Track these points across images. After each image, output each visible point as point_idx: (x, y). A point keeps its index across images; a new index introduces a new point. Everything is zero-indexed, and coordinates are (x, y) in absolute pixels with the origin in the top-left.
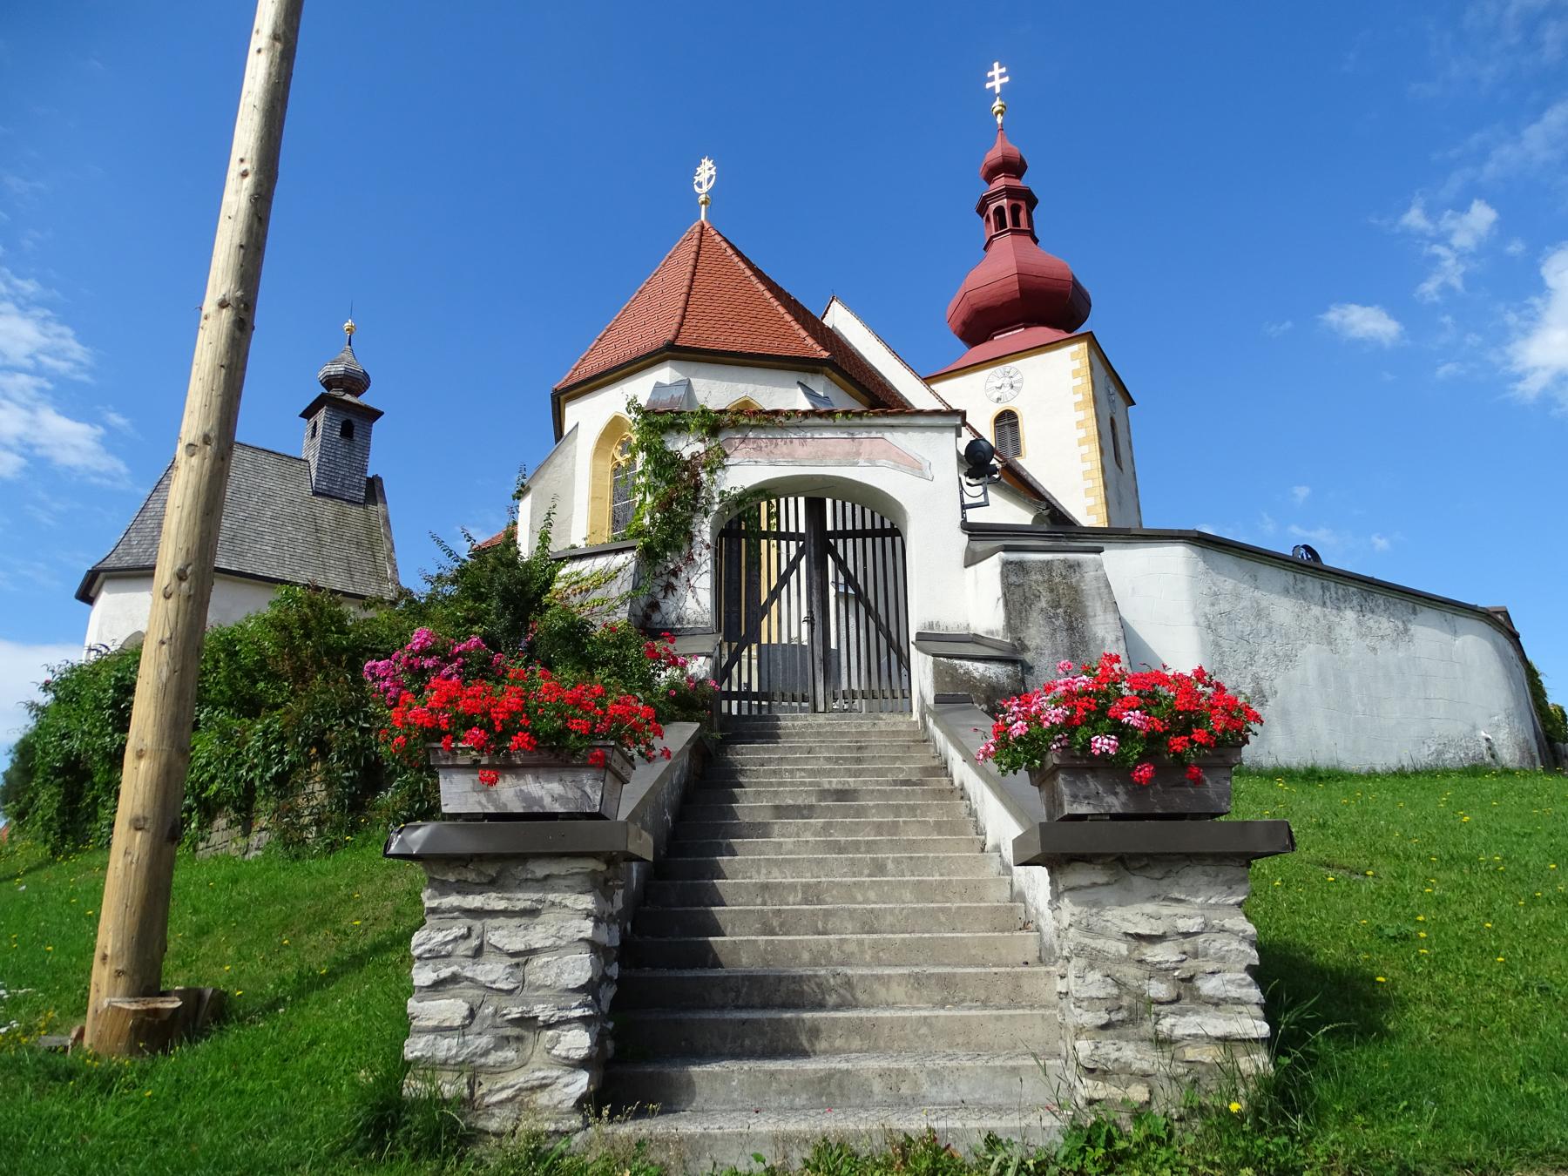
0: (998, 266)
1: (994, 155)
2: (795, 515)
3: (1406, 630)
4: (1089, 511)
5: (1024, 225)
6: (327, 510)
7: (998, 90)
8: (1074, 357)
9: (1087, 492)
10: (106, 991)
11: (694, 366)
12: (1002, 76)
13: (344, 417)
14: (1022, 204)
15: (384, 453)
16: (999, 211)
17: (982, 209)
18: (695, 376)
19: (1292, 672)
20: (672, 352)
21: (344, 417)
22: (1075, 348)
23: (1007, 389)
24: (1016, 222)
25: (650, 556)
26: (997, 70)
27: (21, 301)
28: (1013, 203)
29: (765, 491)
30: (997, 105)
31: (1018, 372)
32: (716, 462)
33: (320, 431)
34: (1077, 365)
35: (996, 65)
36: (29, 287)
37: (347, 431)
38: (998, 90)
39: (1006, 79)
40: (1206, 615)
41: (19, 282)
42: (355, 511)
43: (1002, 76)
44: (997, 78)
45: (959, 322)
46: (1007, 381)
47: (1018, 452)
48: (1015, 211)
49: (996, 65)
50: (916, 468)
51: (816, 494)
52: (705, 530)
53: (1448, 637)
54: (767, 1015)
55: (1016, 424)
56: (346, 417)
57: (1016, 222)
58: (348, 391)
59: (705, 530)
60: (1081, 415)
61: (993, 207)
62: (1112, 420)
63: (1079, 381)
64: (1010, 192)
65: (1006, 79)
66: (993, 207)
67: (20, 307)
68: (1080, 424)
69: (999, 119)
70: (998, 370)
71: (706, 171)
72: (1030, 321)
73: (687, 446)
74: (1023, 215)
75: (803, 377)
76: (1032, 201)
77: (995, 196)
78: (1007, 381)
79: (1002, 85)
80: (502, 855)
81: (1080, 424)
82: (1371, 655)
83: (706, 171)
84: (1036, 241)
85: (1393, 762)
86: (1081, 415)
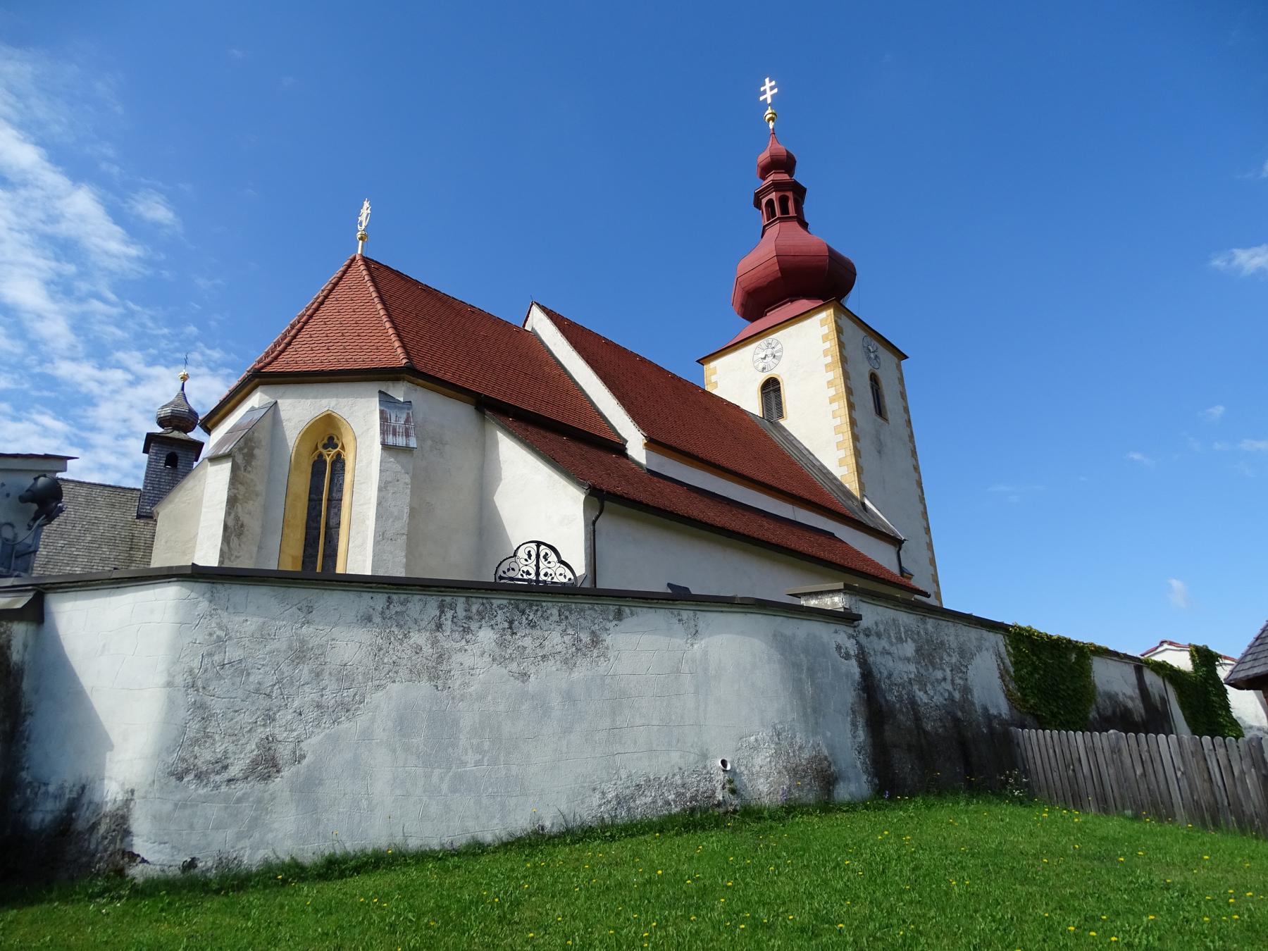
0: (761, 250)
1: (764, 157)
3: (596, 640)
4: (841, 462)
5: (792, 212)
7: (769, 101)
8: (823, 323)
9: (839, 446)
11: (281, 389)
12: (772, 88)
14: (790, 194)
16: (770, 202)
17: (758, 204)
18: (281, 397)
19: (346, 725)
22: (823, 315)
23: (769, 359)
24: (785, 210)
26: (768, 84)
27: (212, 365)
28: (784, 193)
30: (768, 113)
31: (778, 342)
34: (825, 330)
35: (767, 80)
36: (216, 354)
38: (769, 101)
39: (776, 91)
40: (191, 671)
41: (208, 352)
43: (772, 88)
44: (769, 90)
45: (738, 305)
46: (769, 352)
47: (781, 415)
48: (783, 201)
49: (767, 80)
53: (678, 641)
55: (779, 390)
56: (171, 451)
57: (785, 210)
58: (176, 428)
60: (831, 376)
61: (764, 201)
62: (874, 379)
63: (827, 345)
64: (776, 186)
65: (776, 91)
66: (764, 201)
67: (211, 369)
68: (830, 384)
69: (771, 125)
70: (762, 343)
72: (794, 296)
74: (791, 205)
75: (383, 386)
76: (800, 192)
77: (765, 191)
78: (769, 352)
79: (772, 96)
81: (830, 384)
82: (518, 684)
84: (804, 225)
85: (520, 823)
86: (831, 376)
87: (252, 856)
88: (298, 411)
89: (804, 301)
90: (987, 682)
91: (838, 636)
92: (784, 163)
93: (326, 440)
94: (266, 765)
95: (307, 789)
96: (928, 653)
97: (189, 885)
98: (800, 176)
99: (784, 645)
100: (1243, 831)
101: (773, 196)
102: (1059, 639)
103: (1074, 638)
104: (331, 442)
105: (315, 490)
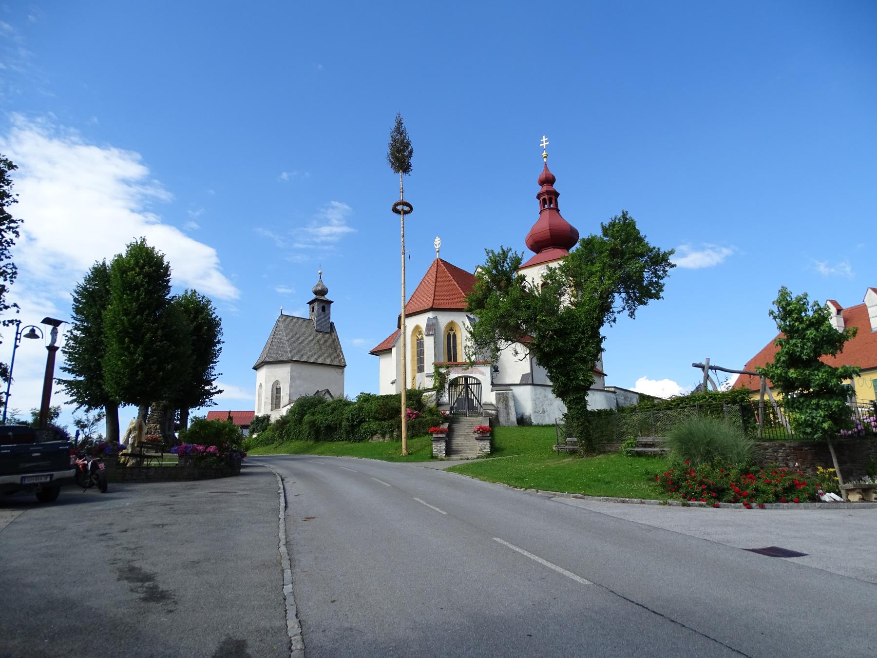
2: (462, 381)
6: (320, 336)
10: (404, 451)
13: (322, 305)
14: (553, 197)
15: (335, 315)
17: (538, 197)
20: (432, 309)
21: (322, 305)
25: (438, 392)
29: (457, 379)
32: (448, 373)
33: (316, 310)
37: (323, 309)
42: (328, 336)
50: (483, 374)
51: (466, 378)
52: (447, 386)
54: (456, 452)
59: (447, 386)
64: (548, 193)
71: (438, 241)
73: (443, 371)
80: (438, 440)
83: (438, 241)
87: (544, 423)
88: (444, 319)
89: (559, 250)
90: (635, 401)
91: (613, 395)
92: (548, 181)
93: (451, 327)
94: (544, 412)
95: (548, 415)
96: (626, 398)
97: (538, 426)
98: (556, 187)
99: (606, 397)
100: (409, 143)
101: (546, 197)
102: (662, 379)
103: (853, 305)
104: (452, 330)
105: (449, 343)
